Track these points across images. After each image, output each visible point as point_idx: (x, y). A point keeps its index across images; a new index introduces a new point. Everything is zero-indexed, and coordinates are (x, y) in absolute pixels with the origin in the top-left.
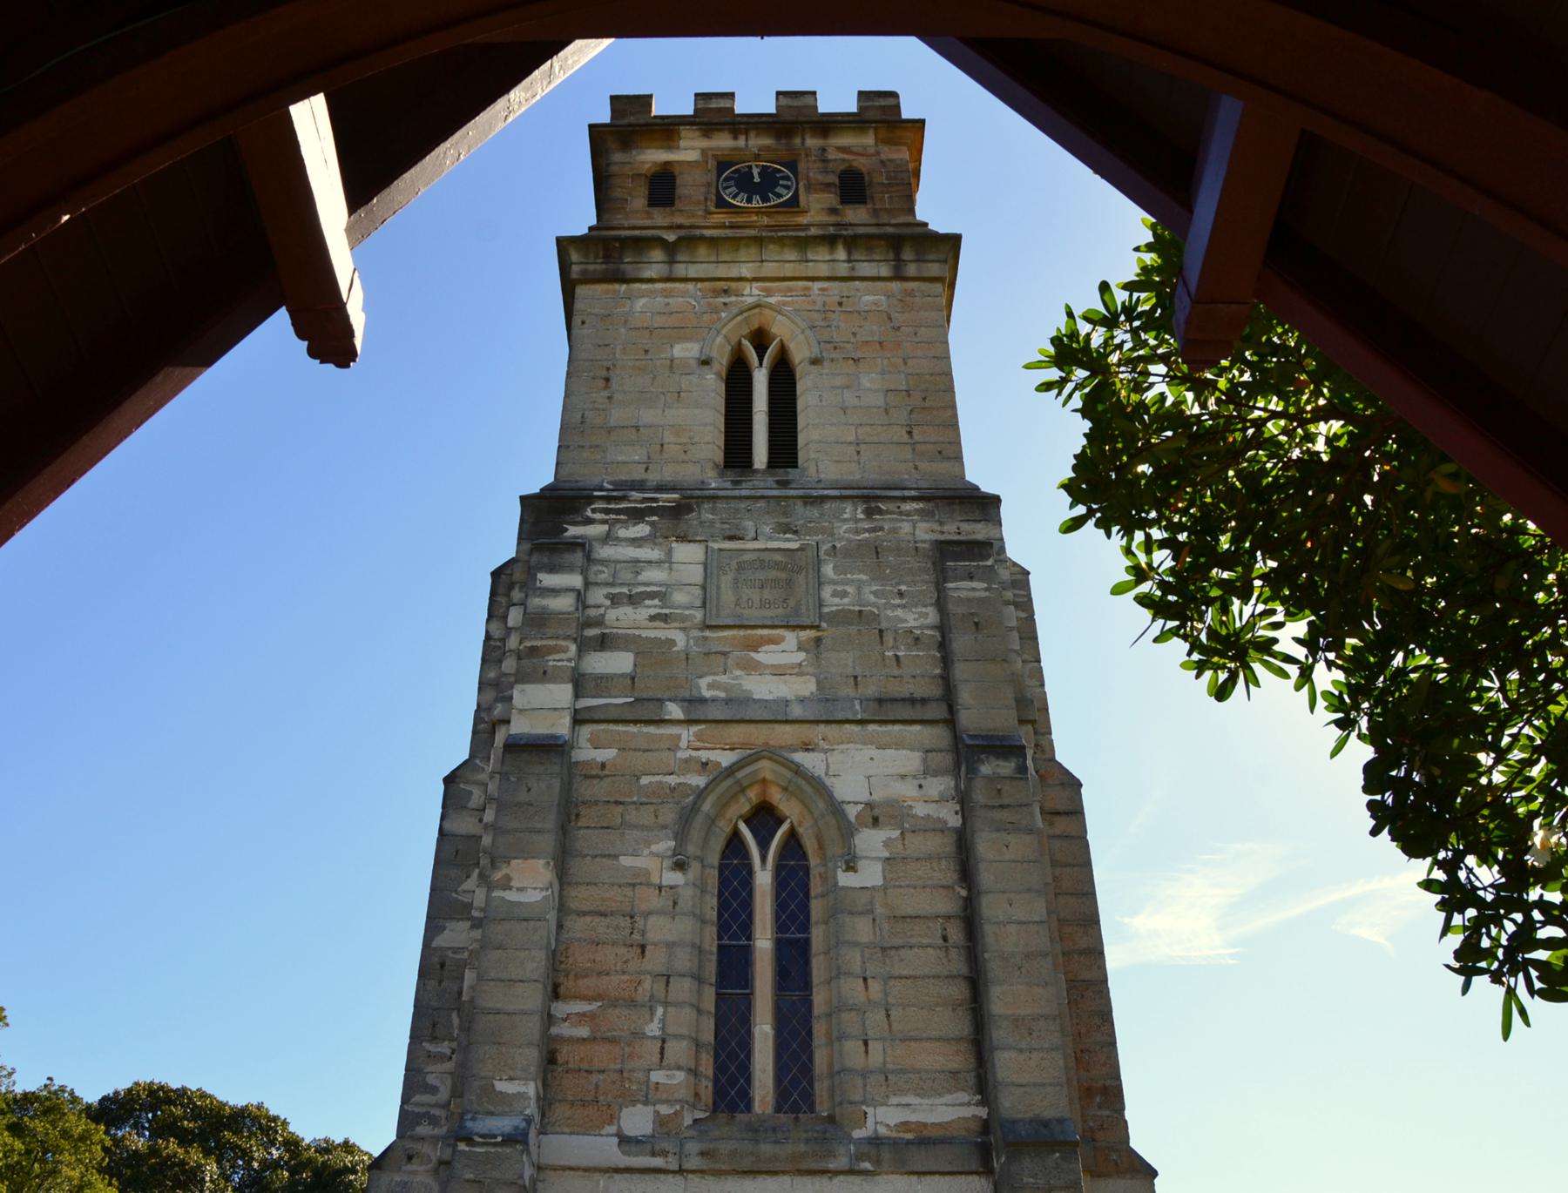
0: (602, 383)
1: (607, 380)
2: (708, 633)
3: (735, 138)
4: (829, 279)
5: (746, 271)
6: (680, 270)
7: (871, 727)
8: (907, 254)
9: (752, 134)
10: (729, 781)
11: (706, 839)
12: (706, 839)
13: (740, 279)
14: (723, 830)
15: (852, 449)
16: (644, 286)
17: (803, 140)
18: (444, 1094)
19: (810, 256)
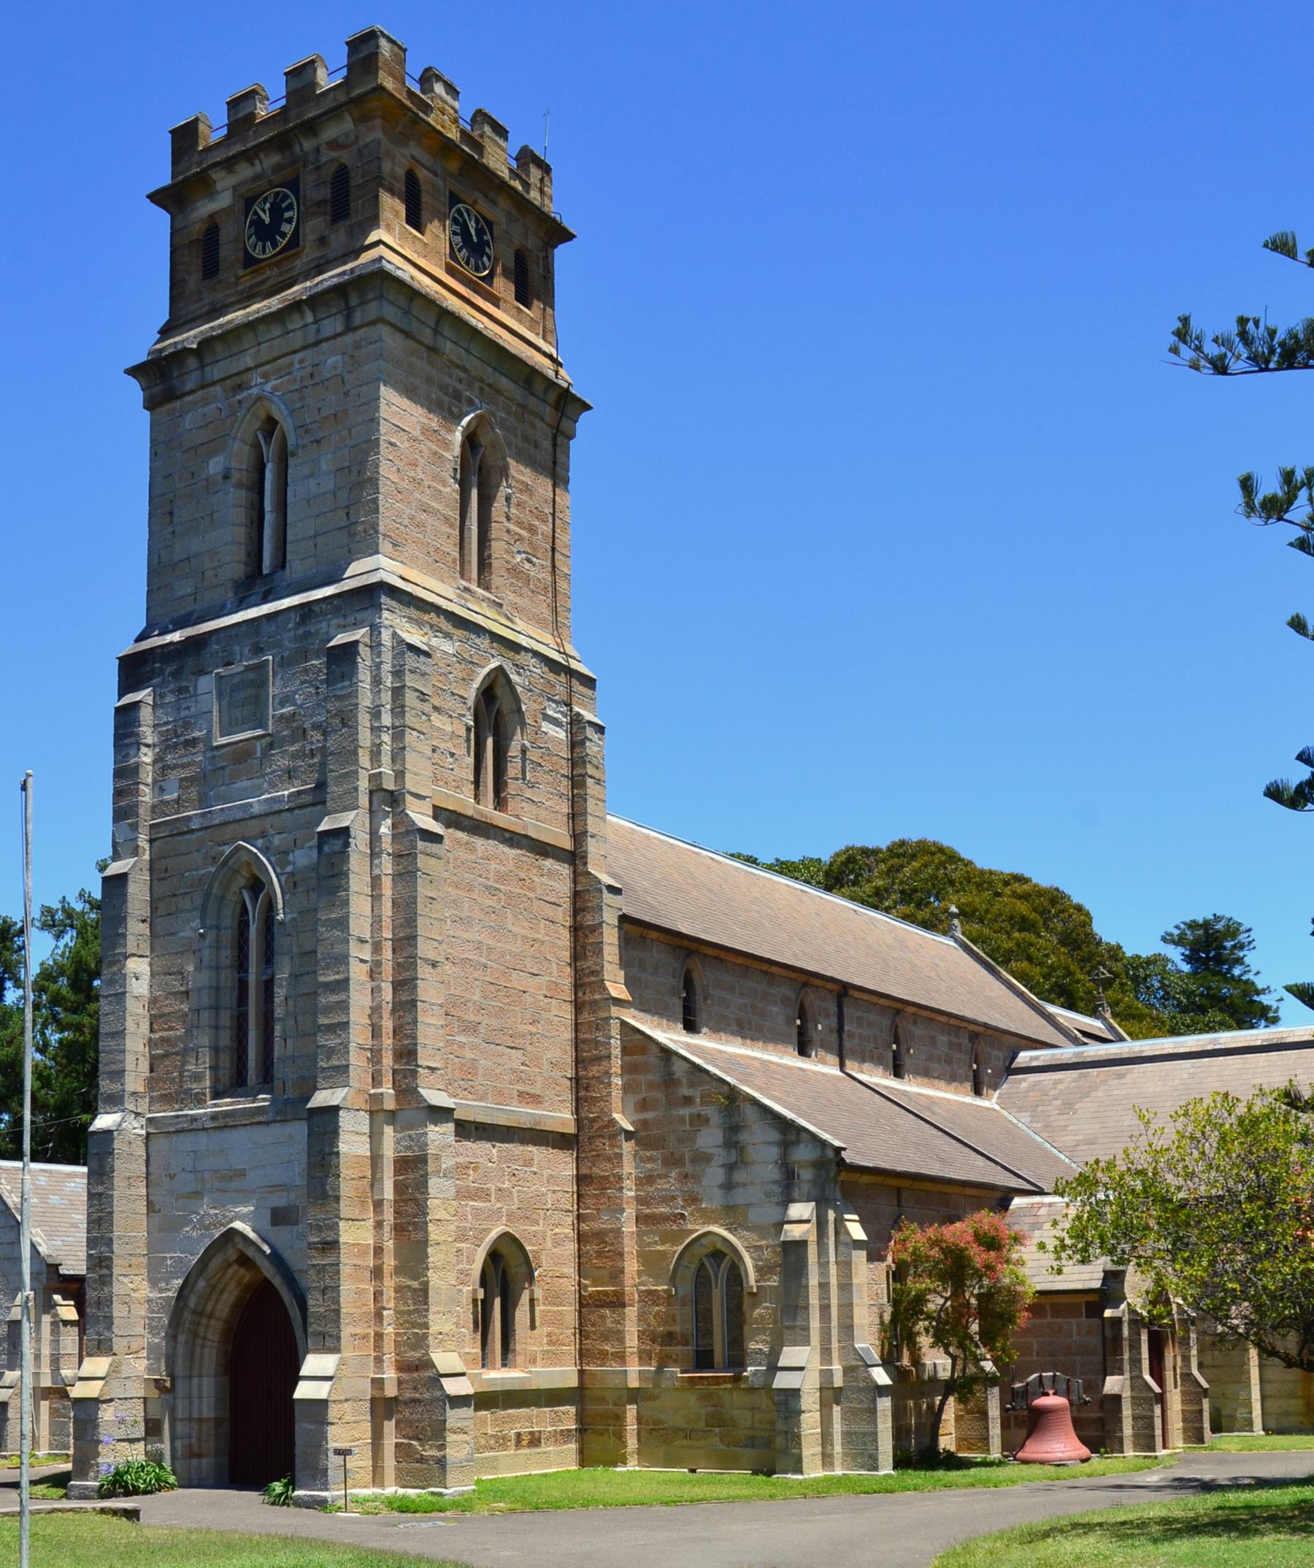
0: (168, 518)
1: (171, 514)
2: (215, 753)
3: (253, 165)
4: (305, 348)
5: (248, 361)
6: (235, 350)
7: (296, 812)
8: (354, 301)
9: (262, 156)
10: (225, 869)
11: (219, 910)
12: (219, 910)
13: (248, 370)
14: (231, 898)
15: (311, 543)
16: (190, 398)
17: (301, 145)
18: (510, 927)
19: (290, 327)
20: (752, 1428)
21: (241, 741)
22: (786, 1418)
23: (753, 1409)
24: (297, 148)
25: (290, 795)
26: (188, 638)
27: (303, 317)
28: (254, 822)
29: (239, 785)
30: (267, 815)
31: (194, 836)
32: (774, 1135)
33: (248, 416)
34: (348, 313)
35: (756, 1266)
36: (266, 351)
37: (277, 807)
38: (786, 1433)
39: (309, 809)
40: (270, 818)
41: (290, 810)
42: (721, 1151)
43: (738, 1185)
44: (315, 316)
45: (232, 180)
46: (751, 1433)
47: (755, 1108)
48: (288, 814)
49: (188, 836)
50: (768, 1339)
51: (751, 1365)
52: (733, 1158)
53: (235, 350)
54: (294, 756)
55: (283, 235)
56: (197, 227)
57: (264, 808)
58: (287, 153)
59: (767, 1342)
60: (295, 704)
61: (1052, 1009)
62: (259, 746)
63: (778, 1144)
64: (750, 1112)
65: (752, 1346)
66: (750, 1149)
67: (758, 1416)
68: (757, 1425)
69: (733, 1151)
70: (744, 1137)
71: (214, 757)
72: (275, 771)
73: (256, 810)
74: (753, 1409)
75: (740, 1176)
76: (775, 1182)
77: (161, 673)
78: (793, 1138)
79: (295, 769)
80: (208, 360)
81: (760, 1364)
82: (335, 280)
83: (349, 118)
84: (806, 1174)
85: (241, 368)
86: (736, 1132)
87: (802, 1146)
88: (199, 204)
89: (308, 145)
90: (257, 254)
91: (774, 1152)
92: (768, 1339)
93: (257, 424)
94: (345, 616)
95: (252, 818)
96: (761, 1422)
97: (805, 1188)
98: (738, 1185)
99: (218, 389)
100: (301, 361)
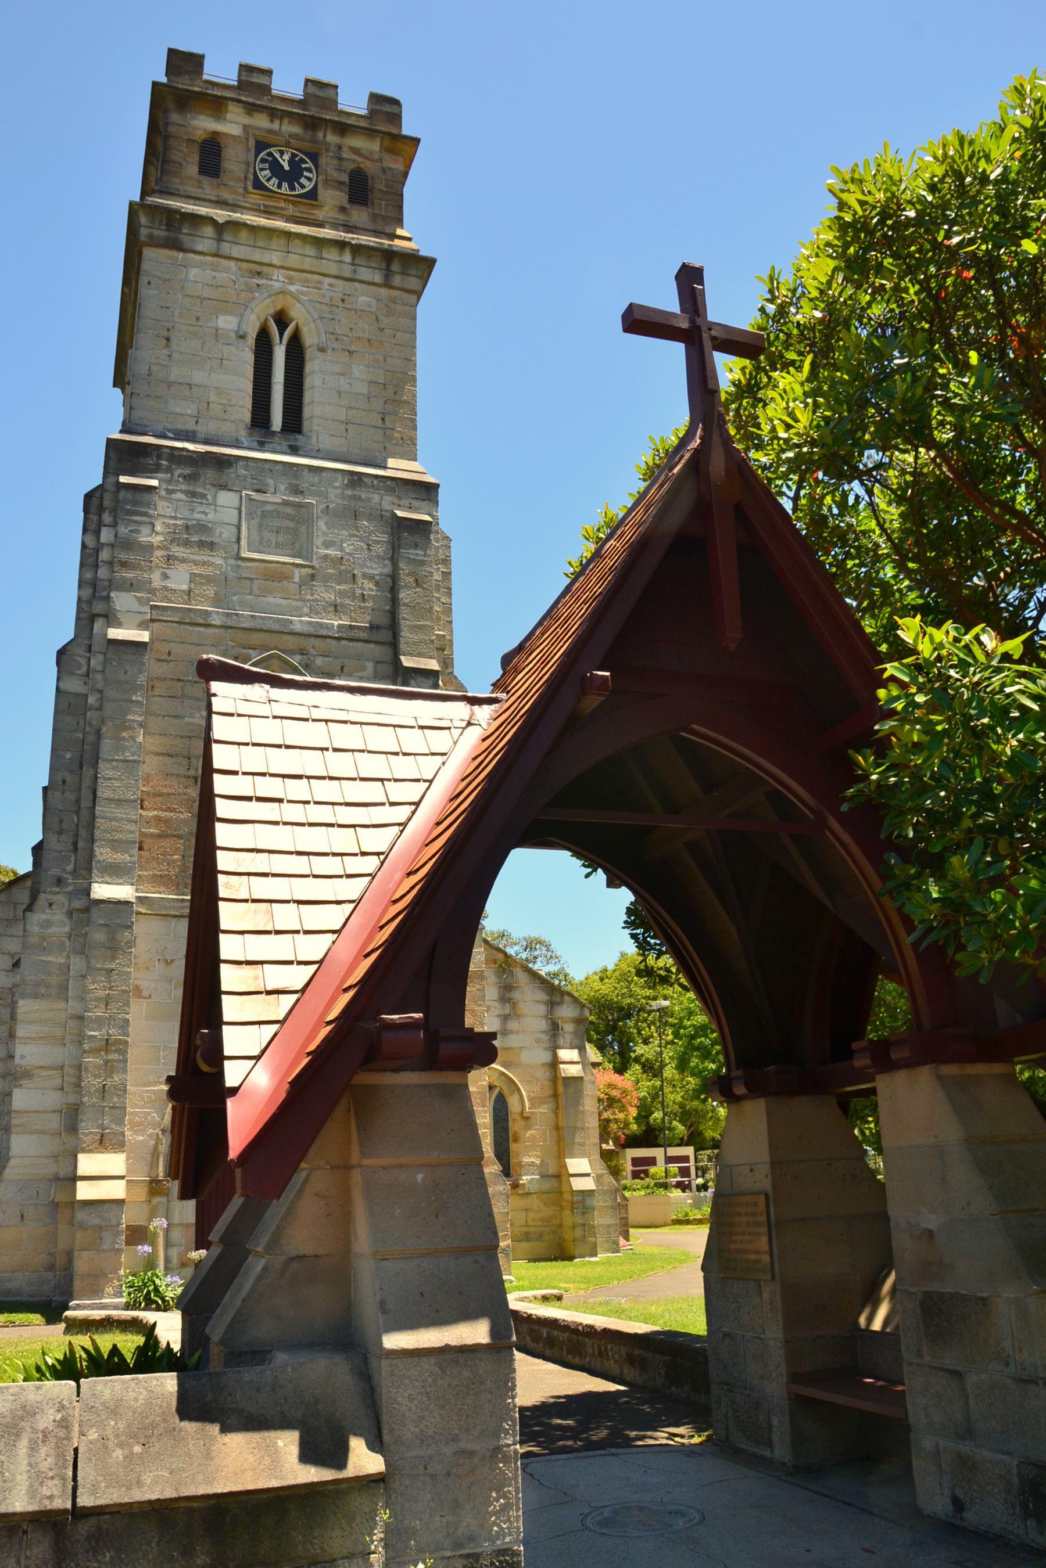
2: (240, 563)
3: (272, 121)
4: (336, 277)
5: (275, 258)
7: (344, 642)
9: (286, 121)
13: (271, 265)
16: (198, 257)
19: (325, 255)
20: (527, 1225)
21: (278, 562)
22: (584, 1213)
23: (526, 1210)
24: (320, 135)
25: (339, 626)
26: (207, 452)
27: (341, 254)
28: (290, 638)
29: (270, 599)
30: (310, 636)
31: (210, 631)
32: (542, 996)
33: (269, 300)
34: (388, 275)
35: (528, 1096)
36: (294, 260)
37: (324, 632)
38: (584, 1225)
39: (360, 644)
40: (312, 639)
41: (338, 639)
42: (496, 1004)
43: (511, 1032)
44: (353, 259)
45: (246, 120)
46: (524, 1230)
47: (526, 974)
48: (334, 642)
49: (202, 629)
50: (539, 1154)
51: (525, 1175)
52: (507, 1012)
53: (261, 244)
54: (342, 594)
55: (279, 186)
56: (200, 133)
57: (306, 629)
58: (309, 132)
59: (538, 1157)
60: (342, 549)
61: (379, 952)
62: (297, 574)
63: (546, 1003)
64: (521, 977)
65: (526, 1160)
66: (521, 1005)
67: (531, 1215)
68: (530, 1223)
69: (507, 1005)
70: (516, 995)
71: (238, 566)
72: (317, 600)
73: (297, 627)
74: (526, 1210)
75: (512, 1025)
76: (544, 1032)
77: (168, 470)
78: (558, 1000)
79: (342, 605)
80: (227, 236)
81: (533, 1174)
82: (372, 244)
83: (379, 144)
84: (569, 1027)
85: (266, 260)
86: (510, 991)
87: (565, 1006)
88: (202, 117)
89: (332, 138)
90: (309, 186)
91: (542, 1009)
92: (539, 1154)
93: (272, 311)
94: (399, 498)
95: (291, 633)
96: (534, 1220)
97: (568, 1038)
98: (511, 1032)
99: (232, 264)
100: (330, 285)
